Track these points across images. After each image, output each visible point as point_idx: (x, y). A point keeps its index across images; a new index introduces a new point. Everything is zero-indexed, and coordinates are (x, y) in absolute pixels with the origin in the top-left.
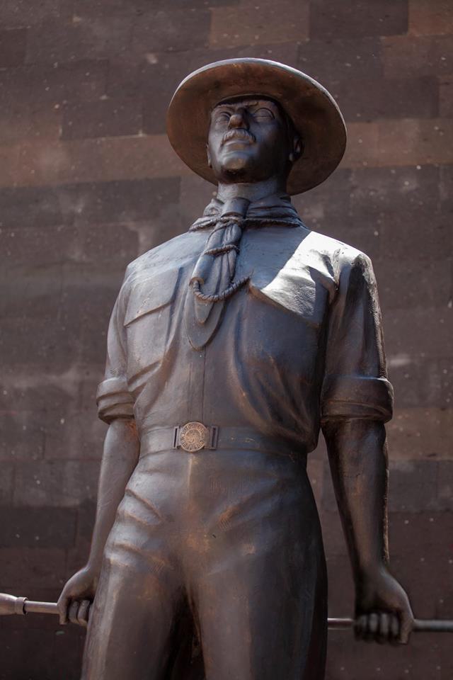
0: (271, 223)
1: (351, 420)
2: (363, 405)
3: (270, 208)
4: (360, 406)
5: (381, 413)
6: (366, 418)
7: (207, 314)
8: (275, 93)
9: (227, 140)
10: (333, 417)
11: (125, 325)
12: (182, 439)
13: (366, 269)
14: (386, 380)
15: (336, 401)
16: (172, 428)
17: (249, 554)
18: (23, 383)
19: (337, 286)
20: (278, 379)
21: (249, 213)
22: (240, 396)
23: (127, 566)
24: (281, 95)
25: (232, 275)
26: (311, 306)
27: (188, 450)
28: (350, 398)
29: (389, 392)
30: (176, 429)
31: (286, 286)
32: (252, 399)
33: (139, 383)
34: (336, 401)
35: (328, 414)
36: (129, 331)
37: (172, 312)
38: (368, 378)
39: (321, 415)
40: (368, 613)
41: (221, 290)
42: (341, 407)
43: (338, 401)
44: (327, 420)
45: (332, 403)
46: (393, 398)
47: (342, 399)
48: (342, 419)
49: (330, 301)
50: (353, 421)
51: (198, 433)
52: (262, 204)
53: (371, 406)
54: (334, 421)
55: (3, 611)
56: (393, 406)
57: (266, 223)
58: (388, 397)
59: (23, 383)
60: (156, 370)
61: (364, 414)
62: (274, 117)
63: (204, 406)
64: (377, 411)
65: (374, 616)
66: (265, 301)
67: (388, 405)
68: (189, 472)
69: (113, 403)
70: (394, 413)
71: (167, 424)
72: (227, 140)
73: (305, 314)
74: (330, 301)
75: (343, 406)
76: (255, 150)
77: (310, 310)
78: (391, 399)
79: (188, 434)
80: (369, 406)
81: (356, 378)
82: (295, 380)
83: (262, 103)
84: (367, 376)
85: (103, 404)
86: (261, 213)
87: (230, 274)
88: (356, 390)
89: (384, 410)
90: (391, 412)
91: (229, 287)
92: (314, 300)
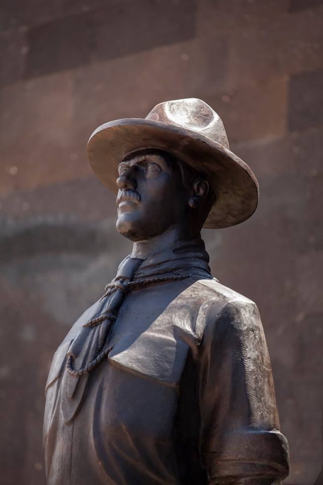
0: (160, 281)
1: (242, 480)
2: (255, 462)
3: (159, 264)
4: (253, 464)
5: (276, 470)
6: (260, 477)
7: (73, 389)
8: (161, 146)
10: (223, 478)
13: (236, 317)
14: (278, 432)
15: (224, 461)
19: (201, 342)
20: (131, 444)
21: (138, 274)
22: (97, 464)
25: (99, 347)
26: (167, 366)
28: (240, 456)
29: (283, 446)
31: (148, 351)
32: (107, 467)
34: (224, 461)
35: (216, 475)
38: (259, 432)
39: (209, 477)
41: (87, 363)
42: (231, 467)
43: (227, 460)
44: (217, 482)
45: (220, 463)
46: (288, 452)
47: (231, 458)
48: (233, 480)
49: (57, 382)
50: (246, 481)
52: (151, 261)
53: (265, 462)
54: (224, 483)
56: (289, 460)
57: (149, 283)
58: (283, 452)
61: (257, 473)
62: (161, 170)
63: (72, 477)
64: (271, 468)
66: (121, 370)
67: (283, 461)
70: (290, 469)
73: (162, 376)
74: (57, 382)
75: (233, 466)
76: (141, 207)
77: (167, 370)
78: (286, 454)
80: (262, 463)
81: (245, 432)
82: (150, 444)
83: (154, 158)
86: (148, 272)
87: (98, 345)
88: (246, 447)
89: (279, 466)
90: (287, 468)
91: (94, 360)
92: (173, 361)
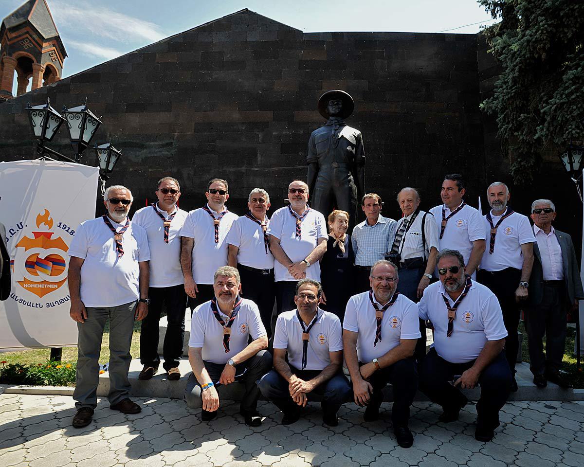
18: (232, 170)
59: (232, 170)
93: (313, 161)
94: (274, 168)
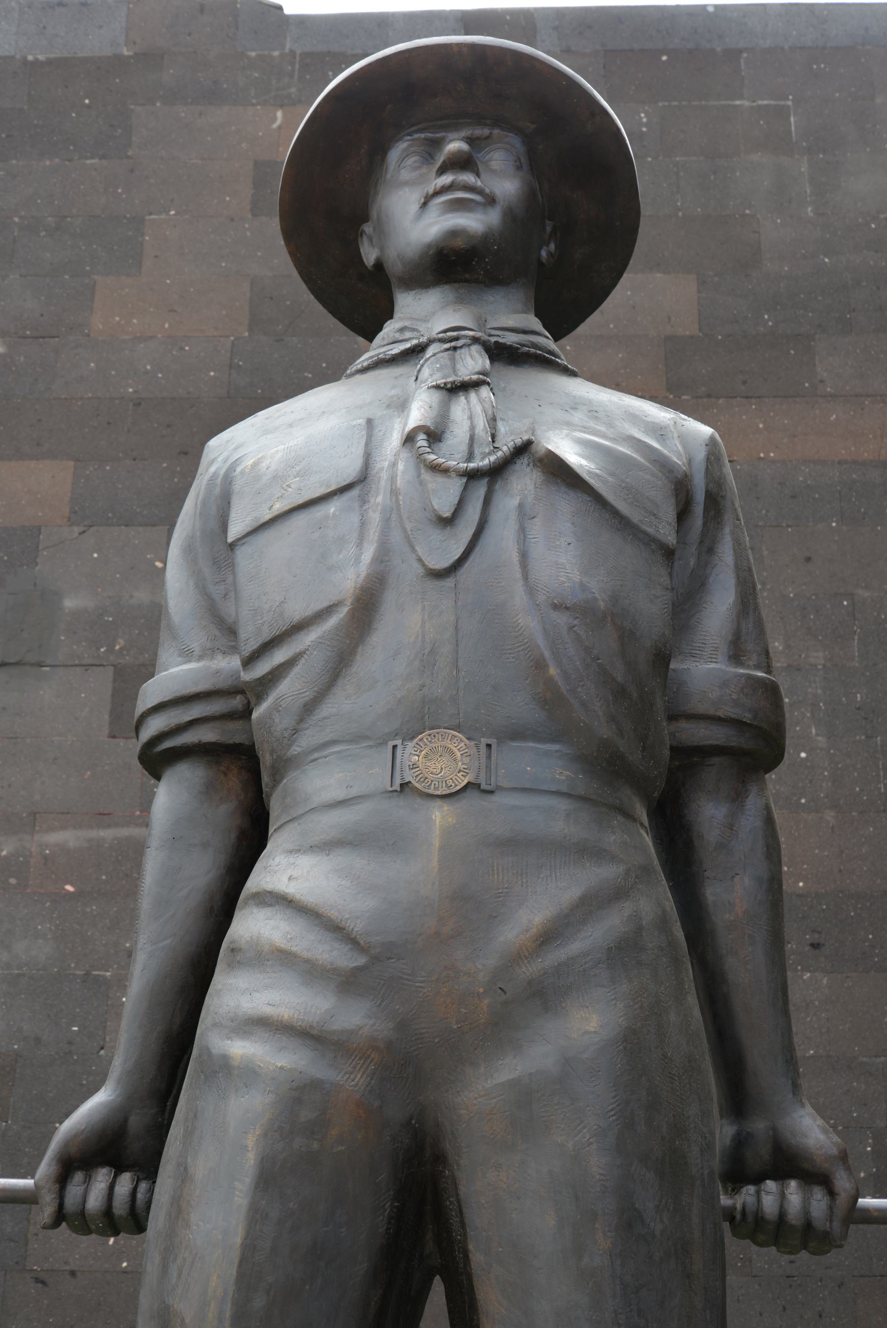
9: (437, 193)
11: (230, 540)
12: (414, 766)
16: (384, 743)
17: (587, 1032)
23: (281, 1068)
24: (533, 126)
27: (431, 791)
30: (395, 747)
33: (279, 656)
36: (243, 555)
37: (363, 500)
40: (758, 1180)
51: (452, 753)
55: (0, 1187)
60: (333, 621)
65: (770, 1185)
68: (437, 842)
69: (187, 718)
71: (367, 738)
72: (437, 193)
79: (425, 757)
84: (748, 667)
85: (155, 726)
93: (207, 735)
94: (56, 837)
